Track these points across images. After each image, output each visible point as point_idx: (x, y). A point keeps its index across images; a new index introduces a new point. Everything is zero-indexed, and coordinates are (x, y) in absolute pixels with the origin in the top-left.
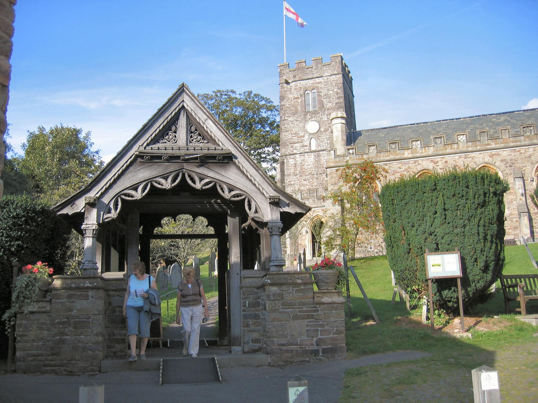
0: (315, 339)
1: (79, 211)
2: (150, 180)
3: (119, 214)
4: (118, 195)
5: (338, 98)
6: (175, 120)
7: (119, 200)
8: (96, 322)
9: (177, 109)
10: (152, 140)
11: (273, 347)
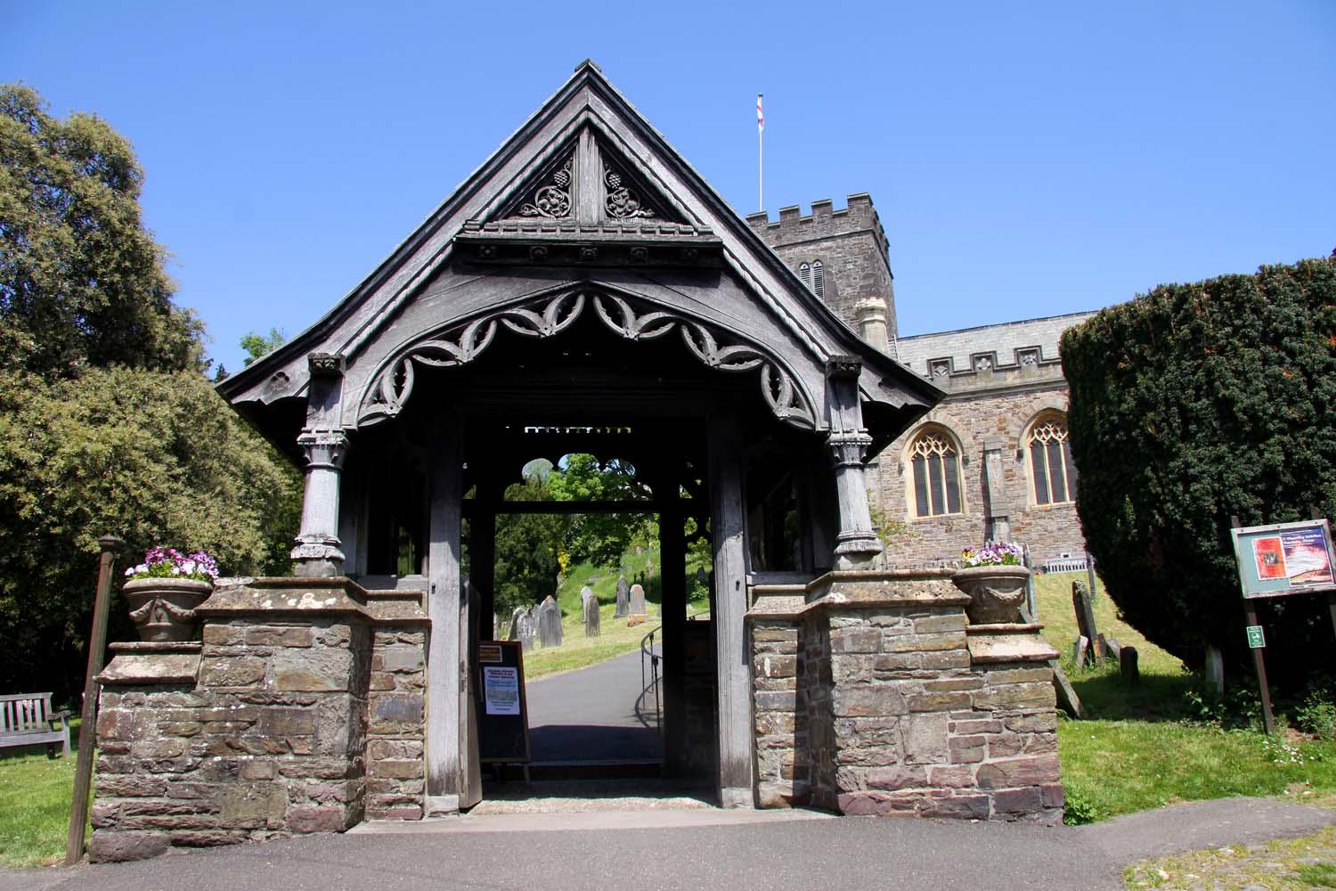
0: (975, 768)
1: (291, 394)
2: (496, 314)
3: (406, 405)
4: (405, 353)
5: (865, 278)
6: (566, 152)
7: (408, 365)
8: (329, 714)
9: (571, 129)
10: (500, 207)
11: (855, 794)
